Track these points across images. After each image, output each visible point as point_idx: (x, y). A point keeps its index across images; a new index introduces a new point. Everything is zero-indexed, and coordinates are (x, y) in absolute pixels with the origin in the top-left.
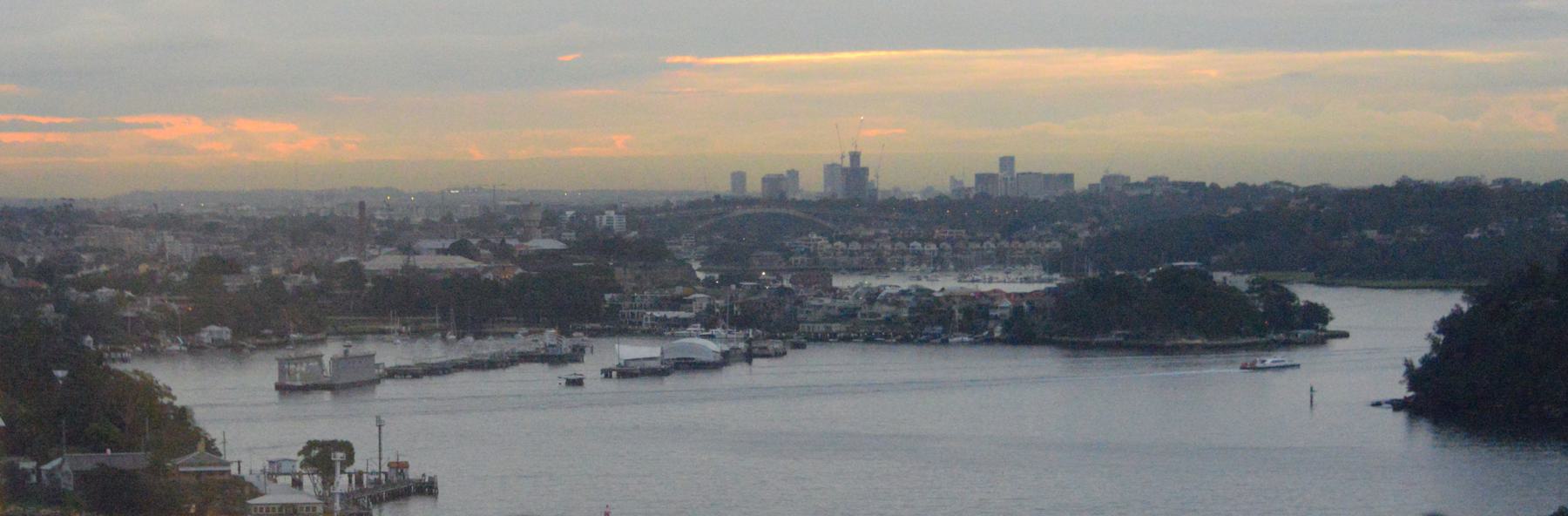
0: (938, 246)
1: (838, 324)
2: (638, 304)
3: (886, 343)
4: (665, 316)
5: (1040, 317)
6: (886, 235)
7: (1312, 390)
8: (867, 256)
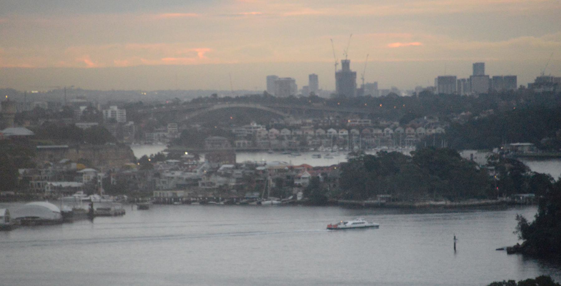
0: (349, 132)
1: (183, 191)
2: (43, 176)
3: (218, 205)
4: (61, 185)
5: (332, 185)
6: (310, 124)
7: (455, 238)
8: (294, 140)
